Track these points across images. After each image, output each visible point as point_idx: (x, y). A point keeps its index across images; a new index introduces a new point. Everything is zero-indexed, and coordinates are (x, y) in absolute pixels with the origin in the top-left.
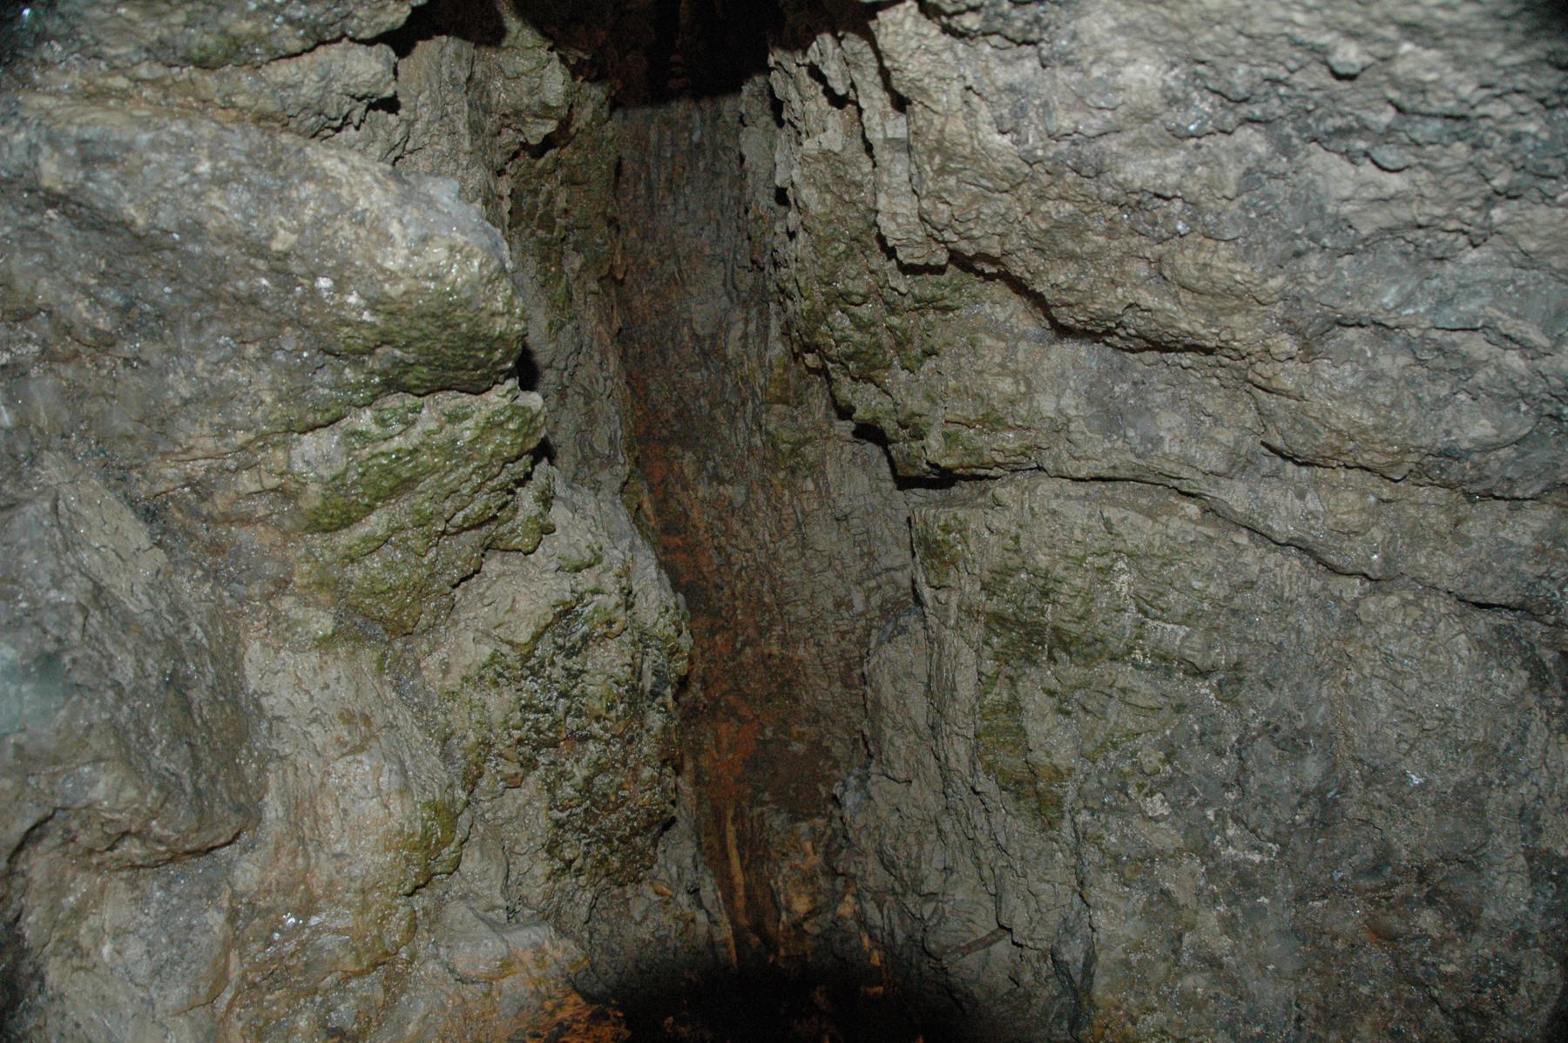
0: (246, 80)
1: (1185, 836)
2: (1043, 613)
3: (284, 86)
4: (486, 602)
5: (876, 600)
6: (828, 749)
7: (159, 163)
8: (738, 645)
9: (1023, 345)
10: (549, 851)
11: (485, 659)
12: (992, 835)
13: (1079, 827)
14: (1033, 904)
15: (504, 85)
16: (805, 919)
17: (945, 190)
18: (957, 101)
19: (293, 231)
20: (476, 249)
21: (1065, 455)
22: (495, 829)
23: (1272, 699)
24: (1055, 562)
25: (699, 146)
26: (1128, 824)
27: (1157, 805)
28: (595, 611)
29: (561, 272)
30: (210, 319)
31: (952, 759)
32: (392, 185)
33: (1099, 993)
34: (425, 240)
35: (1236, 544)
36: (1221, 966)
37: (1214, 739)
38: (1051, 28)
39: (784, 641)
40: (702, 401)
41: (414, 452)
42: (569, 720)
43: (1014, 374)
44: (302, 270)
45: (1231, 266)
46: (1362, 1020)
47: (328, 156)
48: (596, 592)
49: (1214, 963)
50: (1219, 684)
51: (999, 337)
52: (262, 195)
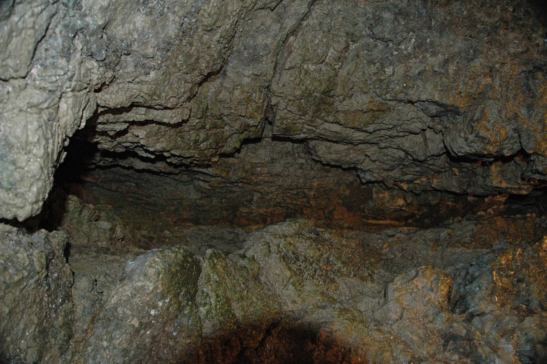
0: (79, 324)
1: (401, 63)
2: (316, 96)
3: (83, 311)
4: (274, 284)
5: (302, 155)
6: (350, 182)
7: (101, 358)
8: (309, 205)
9: (225, 85)
10: (364, 281)
11: (293, 288)
12: (389, 129)
13: (391, 98)
14: (415, 120)
15: (100, 242)
16: (406, 201)
17: (166, 97)
18: (136, 86)
19: (133, 318)
20: (152, 258)
21: (265, 78)
22: (353, 297)
23: (361, 25)
24: (300, 89)
25: (136, 184)
26: (393, 81)
27: (389, 70)
28: (285, 248)
29: (169, 238)
30: (157, 354)
31: (360, 138)
32: (125, 282)
33: (449, 102)
34: (145, 275)
35: (306, 26)
36: (448, 59)
37: (370, 47)
38: (118, 48)
39: (310, 189)
40: (223, 201)
41: (217, 296)
42: (320, 265)
43: (233, 89)
44: (147, 318)
45: (211, 6)
46: (475, 15)
47: (110, 301)
48: (279, 246)
49: (446, 62)
50: (352, 41)
51: (220, 92)
52: (118, 327)
